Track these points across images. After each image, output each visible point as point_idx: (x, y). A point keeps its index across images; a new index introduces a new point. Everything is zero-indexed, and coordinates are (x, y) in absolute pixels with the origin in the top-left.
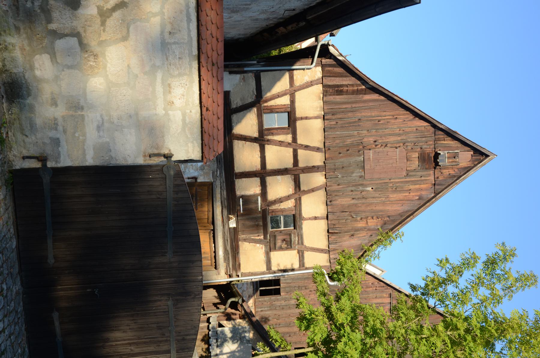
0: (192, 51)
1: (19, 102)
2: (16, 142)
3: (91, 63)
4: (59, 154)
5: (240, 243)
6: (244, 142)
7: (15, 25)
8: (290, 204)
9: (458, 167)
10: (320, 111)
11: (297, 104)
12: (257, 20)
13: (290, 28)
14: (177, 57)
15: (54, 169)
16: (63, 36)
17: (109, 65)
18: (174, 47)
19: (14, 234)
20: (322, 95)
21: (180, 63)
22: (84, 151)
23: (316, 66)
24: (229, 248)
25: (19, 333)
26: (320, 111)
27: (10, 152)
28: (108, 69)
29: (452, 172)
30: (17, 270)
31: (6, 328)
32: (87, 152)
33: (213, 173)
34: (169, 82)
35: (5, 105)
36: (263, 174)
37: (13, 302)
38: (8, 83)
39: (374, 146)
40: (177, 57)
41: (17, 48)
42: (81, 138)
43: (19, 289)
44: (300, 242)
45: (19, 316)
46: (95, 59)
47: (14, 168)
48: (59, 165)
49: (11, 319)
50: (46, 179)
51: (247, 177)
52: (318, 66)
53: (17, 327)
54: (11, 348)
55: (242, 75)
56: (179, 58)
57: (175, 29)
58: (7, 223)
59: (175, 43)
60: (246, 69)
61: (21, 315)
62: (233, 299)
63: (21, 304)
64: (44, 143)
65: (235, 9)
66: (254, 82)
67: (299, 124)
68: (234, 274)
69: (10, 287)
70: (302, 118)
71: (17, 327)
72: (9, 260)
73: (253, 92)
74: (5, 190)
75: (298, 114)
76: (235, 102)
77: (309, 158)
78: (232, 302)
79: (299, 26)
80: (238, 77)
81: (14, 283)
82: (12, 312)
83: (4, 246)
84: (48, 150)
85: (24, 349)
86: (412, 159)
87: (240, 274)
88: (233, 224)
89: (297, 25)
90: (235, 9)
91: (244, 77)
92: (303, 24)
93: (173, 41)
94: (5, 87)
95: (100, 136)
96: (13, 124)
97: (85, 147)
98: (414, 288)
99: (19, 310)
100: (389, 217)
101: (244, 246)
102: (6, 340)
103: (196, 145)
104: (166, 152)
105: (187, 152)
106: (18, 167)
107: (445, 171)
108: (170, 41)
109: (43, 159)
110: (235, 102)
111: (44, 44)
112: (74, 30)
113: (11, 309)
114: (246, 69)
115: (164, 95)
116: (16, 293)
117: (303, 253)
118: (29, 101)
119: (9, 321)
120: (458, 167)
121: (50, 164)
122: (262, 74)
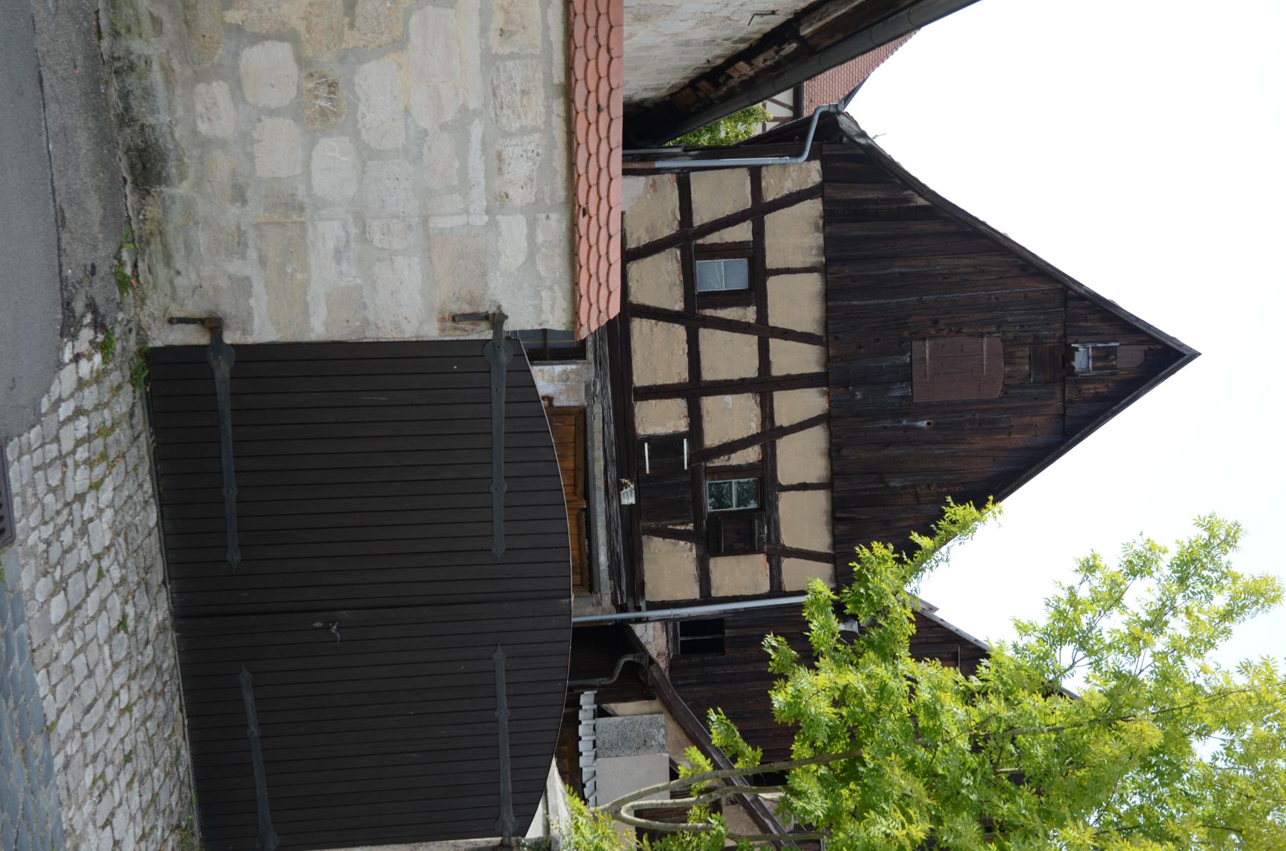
0: (551, 75)
1: (161, 192)
2: (155, 287)
3: (322, 103)
4: (250, 314)
5: (644, 538)
6: (653, 322)
7: (151, 14)
8: (751, 455)
9: (1115, 378)
10: (817, 255)
11: (769, 241)
12: (687, 43)
13: (760, 62)
14: (518, 88)
15: (236, 347)
16: (258, 38)
17: (362, 108)
18: (510, 64)
19: (154, 496)
20: (821, 222)
21: (525, 102)
22: (306, 305)
23: (808, 159)
24: (619, 549)
25: (165, 717)
26: (817, 255)
27: (142, 309)
28: (359, 116)
29: (1102, 389)
30: (161, 578)
31: (135, 704)
32: (311, 309)
33: (587, 387)
34: (498, 147)
35: (131, 200)
36: (694, 390)
37: (150, 647)
38: (137, 149)
39: (933, 332)
40: (518, 88)
41: (155, 66)
42: (299, 276)
43: (164, 620)
44: (773, 537)
45: (166, 677)
46: (330, 93)
47: (150, 345)
48: (250, 340)
49: (147, 683)
50: (223, 370)
51: (661, 398)
52: (814, 159)
53: (160, 703)
54: (147, 748)
55: (651, 177)
56: (523, 91)
57: (512, 23)
58: (135, 469)
59: (512, 56)
60: (658, 164)
61: (171, 677)
62: (629, 658)
63: (170, 651)
64: (216, 289)
65: (642, 12)
66: (676, 192)
67: (773, 283)
68: (630, 605)
69: (142, 613)
70: (778, 272)
71: (160, 703)
72: (141, 553)
73: (674, 214)
74: (131, 394)
75: (771, 261)
76: (635, 237)
77: (792, 358)
78: (626, 663)
79: (782, 53)
80: (641, 181)
81: (154, 606)
82: (147, 668)
83: (128, 519)
84: (226, 307)
85: (178, 753)
86: (1016, 361)
87: (642, 604)
88: (629, 498)
89: (777, 52)
90: (642, 12)
91: (654, 182)
92: (791, 47)
93: (507, 50)
94: (130, 158)
95: (341, 273)
96: (148, 244)
97: (309, 298)
98: (1023, 629)
99: (165, 666)
100: (963, 484)
101: (653, 545)
102: (138, 730)
103: (559, 294)
104: (492, 310)
105: (539, 310)
106: (158, 344)
107: (1086, 386)
108: (501, 51)
109: (213, 324)
110: (635, 237)
111: (217, 57)
112: (284, 24)
113: (147, 661)
114: (658, 164)
115: (486, 177)
116: (158, 625)
117: (779, 563)
118: (182, 189)
119: (141, 687)
120: (1115, 378)
121: (230, 338)
122: (692, 175)
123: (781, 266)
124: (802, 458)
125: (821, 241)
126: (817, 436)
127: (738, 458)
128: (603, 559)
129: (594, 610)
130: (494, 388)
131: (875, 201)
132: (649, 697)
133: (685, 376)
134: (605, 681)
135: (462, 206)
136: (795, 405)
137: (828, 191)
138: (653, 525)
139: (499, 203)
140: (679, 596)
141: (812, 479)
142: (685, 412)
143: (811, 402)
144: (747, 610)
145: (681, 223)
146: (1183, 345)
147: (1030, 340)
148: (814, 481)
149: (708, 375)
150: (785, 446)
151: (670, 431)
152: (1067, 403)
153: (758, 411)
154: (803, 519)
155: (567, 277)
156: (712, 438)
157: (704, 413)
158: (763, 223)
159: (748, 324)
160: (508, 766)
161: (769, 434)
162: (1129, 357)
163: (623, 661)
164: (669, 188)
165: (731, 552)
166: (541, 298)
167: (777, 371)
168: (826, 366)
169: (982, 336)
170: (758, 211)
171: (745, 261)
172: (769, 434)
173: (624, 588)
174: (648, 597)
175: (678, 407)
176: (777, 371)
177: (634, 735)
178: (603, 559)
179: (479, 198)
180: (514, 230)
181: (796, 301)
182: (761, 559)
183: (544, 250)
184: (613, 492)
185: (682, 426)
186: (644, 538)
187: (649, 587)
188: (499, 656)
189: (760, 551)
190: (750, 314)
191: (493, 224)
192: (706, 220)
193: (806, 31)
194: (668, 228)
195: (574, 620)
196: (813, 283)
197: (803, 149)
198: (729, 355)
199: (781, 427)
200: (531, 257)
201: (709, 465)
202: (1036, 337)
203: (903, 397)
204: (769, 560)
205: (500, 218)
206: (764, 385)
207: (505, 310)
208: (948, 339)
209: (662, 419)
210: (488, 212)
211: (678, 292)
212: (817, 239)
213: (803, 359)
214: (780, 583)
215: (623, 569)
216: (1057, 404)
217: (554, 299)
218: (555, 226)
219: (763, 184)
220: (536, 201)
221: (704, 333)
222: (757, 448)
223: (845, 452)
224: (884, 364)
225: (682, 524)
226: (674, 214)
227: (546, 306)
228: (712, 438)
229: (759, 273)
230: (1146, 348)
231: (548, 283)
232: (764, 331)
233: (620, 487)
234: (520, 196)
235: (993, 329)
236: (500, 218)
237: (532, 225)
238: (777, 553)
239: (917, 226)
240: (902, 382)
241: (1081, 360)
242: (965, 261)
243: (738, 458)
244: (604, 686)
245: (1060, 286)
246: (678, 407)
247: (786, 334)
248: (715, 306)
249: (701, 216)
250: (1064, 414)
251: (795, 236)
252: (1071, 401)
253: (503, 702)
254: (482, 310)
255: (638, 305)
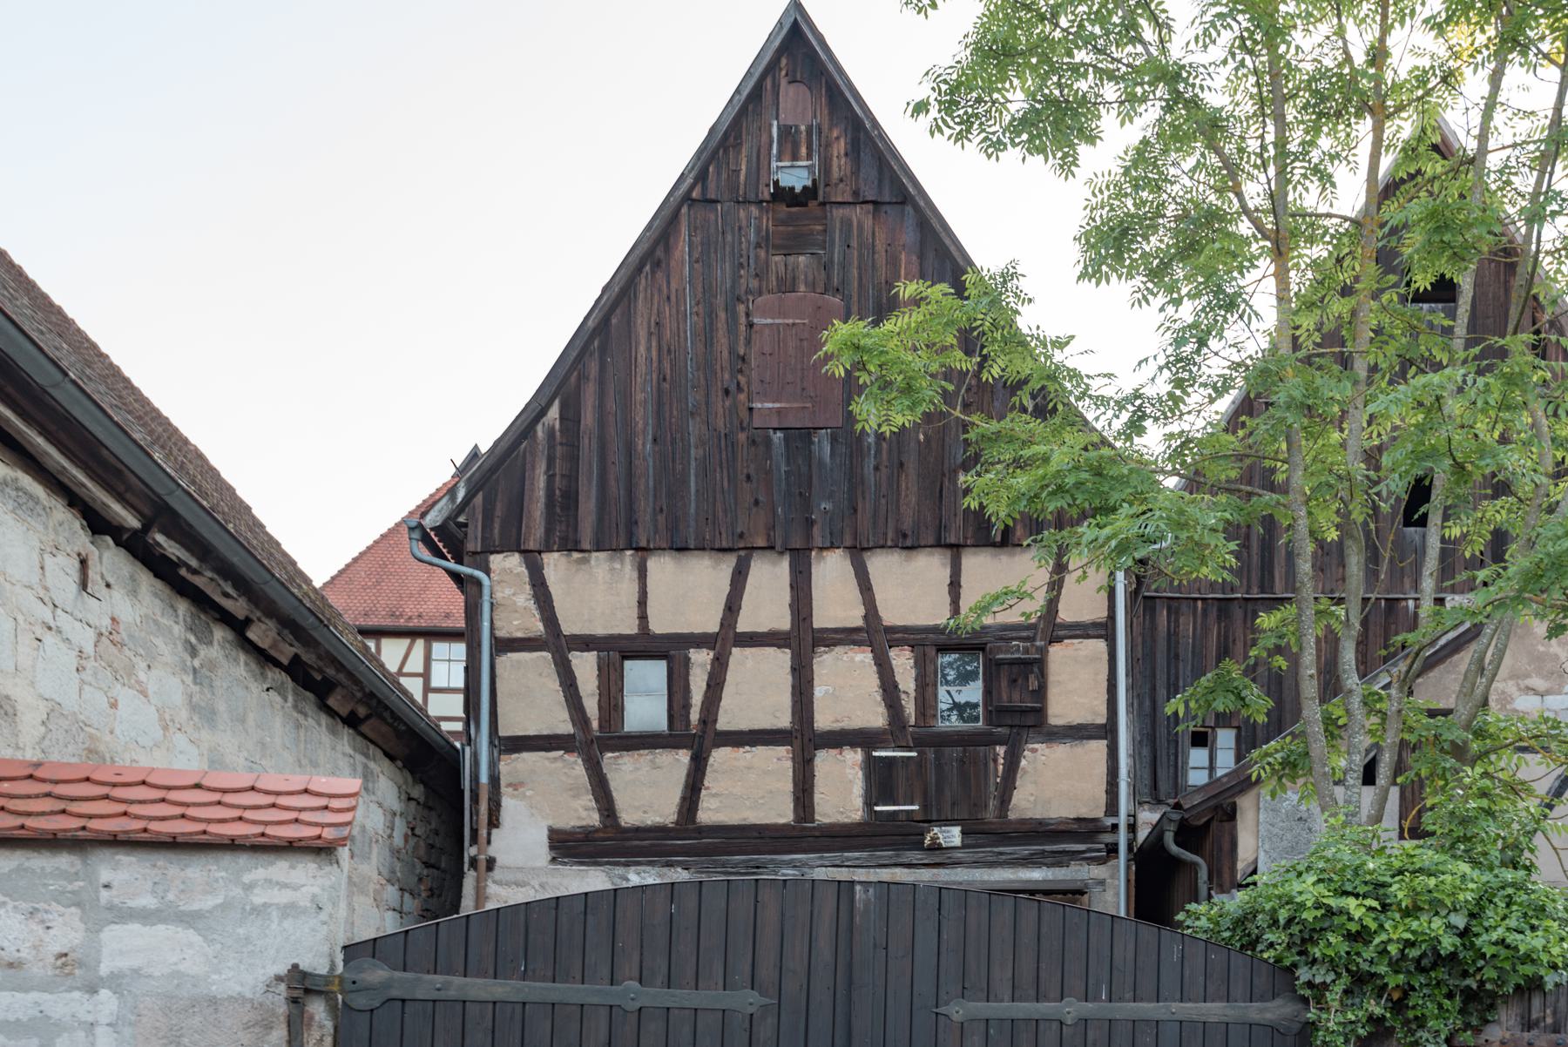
5: (1012, 816)
6: (703, 792)
8: (903, 662)
9: (825, 127)
20: (576, 555)
23: (488, 572)
24: (1024, 850)
29: (840, 147)
36: (804, 739)
39: (742, 397)
44: (1024, 634)
52: (487, 562)
55: (503, 789)
60: (484, 778)
66: (525, 755)
67: (658, 626)
68: (1108, 838)
70: (643, 617)
73: (555, 759)
75: (629, 627)
77: (767, 602)
78: (1177, 843)
80: (509, 803)
87: (1109, 821)
88: (952, 836)
91: (509, 785)
101: (1024, 804)
107: (835, 169)
110: (584, 814)
114: (484, 778)
115: (27, 991)
120: (825, 127)
123: (634, 612)
124: (912, 588)
125: (602, 555)
126: (882, 565)
127: (906, 678)
128: (1036, 875)
129: (1112, 888)
130: (435, 995)
131: (550, 478)
132: (1231, 815)
133: (783, 751)
134: (1203, 874)
135: (81, 1034)
136: (835, 594)
137: (532, 545)
138: (992, 803)
139: (72, 969)
140: (1102, 769)
141: (945, 574)
142: (833, 752)
143: (832, 573)
144: (1130, 672)
145: (568, 750)
146: (780, 22)
147: (762, 253)
148: (947, 572)
149: (784, 720)
150: (893, 613)
151: (860, 774)
152: (858, 200)
153: (839, 650)
154: (1002, 585)
155: (227, 859)
156: (877, 718)
157: (837, 726)
158: (574, 637)
159: (716, 659)
160: (1175, 1006)
161: (875, 635)
162: (795, 105)
163: (1174, 849)
164: (520, 766)
165: (1041, 693)
166: (265, 905)
167: (784, 623)
168: (781, 553)
169: (751, 325)
170: (557, 643)
171: (628, 664)
172: (875, 635)
173: (1082, 847)
174: (1100, 813)
175: (824, 761)
176: (784, 623)
177: (1289, 836)
178: (1036, 875)
179: (65, 1004)
180: (123, 946)
181: (687, 591)
182: (1055, 651)
183: (171, 896)
184: (940, 856)
185: (854, 757)
186: (1012, 816)
187: (1085, 812)
188: (957, 1011)
189: (1044, 652)
190: (701, 659)
191: (115, 982)
192: (565, 715)
193: (133, 522)
194: (573, 768)
195: (1122, 914)
196: (662, 568)
197: (471, 577)
198: (757, 690)
199: (865, 617)
200: (188, 919)
201: (912, 721)
202: (758, 245)
203: (834, 440)
204: (1059, 640)
205: (104, 970)
206: (803, 641)
207: (282, 969)
208: (754, 374)
209: (842, 789)
210: (92, 990)
211: (665, 757)
212: (600, 562)
213: (769, 583)
214: (1095, 625)
215: (1048, 848)
216: (857, 214)
217: (269, 882)
218: (123, 874)
219: (519, 635)
220: (78, 905)
221: (724, 723)
222: (893, 653)
223: (907, 525)
224: (784, 468)
225: (995, 761)
226: (555, 759)
227: (284, 897)
228: (877, 718)
229: (645, 645)
230: (784, 82)
231: (237, 891)
232: (726, 639)
233: (936, 847)
234: (66, 932)
235: (741, 308)
236: (104, 970)
237: (124, 915)
238: (1052, 629)
239: (588, 418)
240: (812, 443)
241: (795, 177)
242: (642, 349)
243: (906, 678)
244: (1210, 878)
245: (684, 210)
246: (824, 761)
247: (732, 607)
248: (687, 706)
249: (562, 724)
250: (874, 203)
251: (594, 593)
252: (856, 193)
253: (1046, 1008)
254: (282, 1009)
255: (680, 812)
